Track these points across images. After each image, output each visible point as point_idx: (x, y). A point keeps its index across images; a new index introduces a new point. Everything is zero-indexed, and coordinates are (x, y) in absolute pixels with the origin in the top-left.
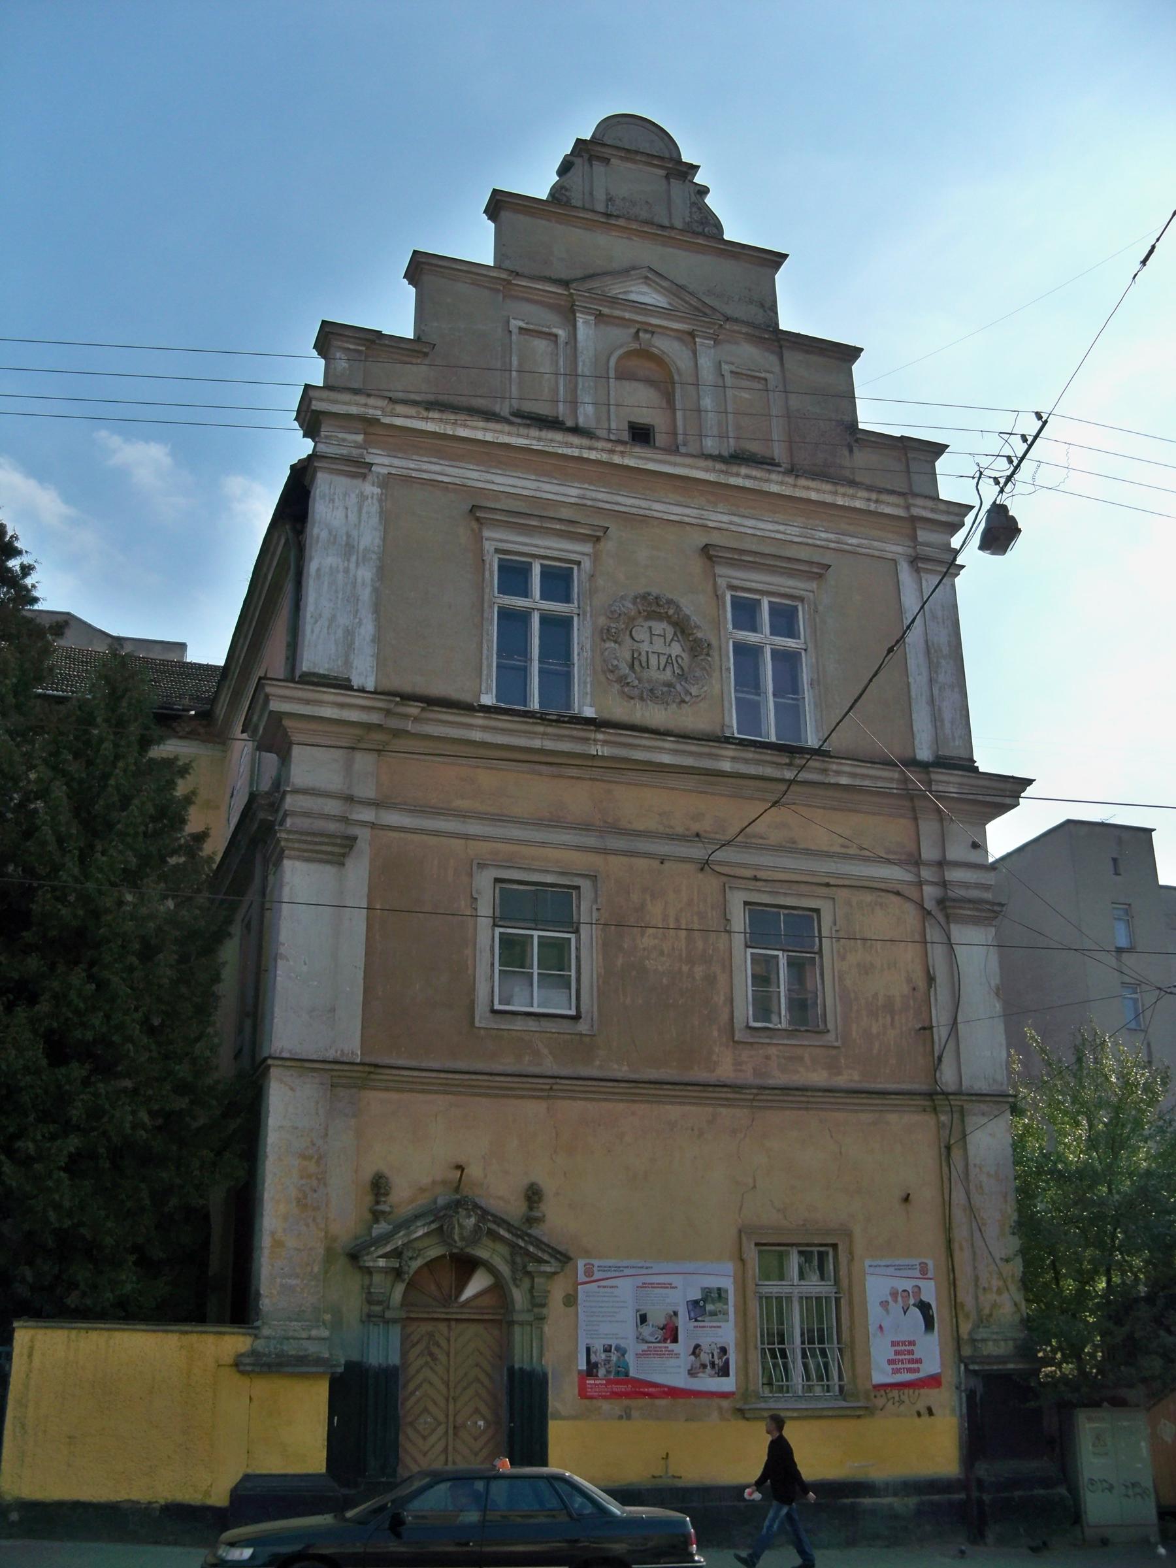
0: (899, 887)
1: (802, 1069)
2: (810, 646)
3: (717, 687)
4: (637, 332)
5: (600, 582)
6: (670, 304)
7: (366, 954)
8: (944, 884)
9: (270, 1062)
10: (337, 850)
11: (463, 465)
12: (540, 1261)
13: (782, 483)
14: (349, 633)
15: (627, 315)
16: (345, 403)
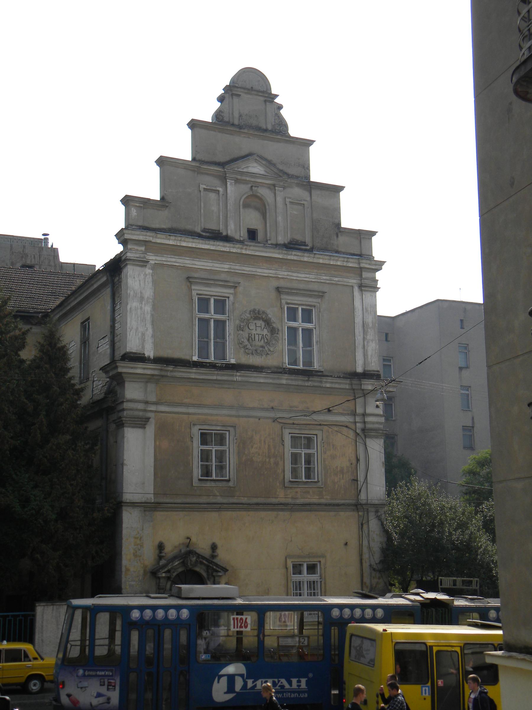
0: (347, 424)
1: (309, 497)
2: (317, 326)
3: (281, 347)
4: (252, 187)
5: (237, 305)
6: (266, 171)
7: (154, 461)
8: (365, 422)
9: (123, 504)
10: (143, 423)
11: (183, 258)
12: (217, 571)
13: (309, 257)
14: (143, 334)
15: (248, 179)
16: (138, 235)
